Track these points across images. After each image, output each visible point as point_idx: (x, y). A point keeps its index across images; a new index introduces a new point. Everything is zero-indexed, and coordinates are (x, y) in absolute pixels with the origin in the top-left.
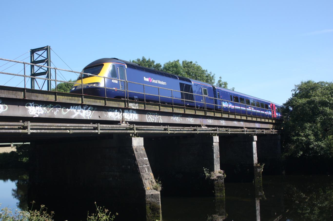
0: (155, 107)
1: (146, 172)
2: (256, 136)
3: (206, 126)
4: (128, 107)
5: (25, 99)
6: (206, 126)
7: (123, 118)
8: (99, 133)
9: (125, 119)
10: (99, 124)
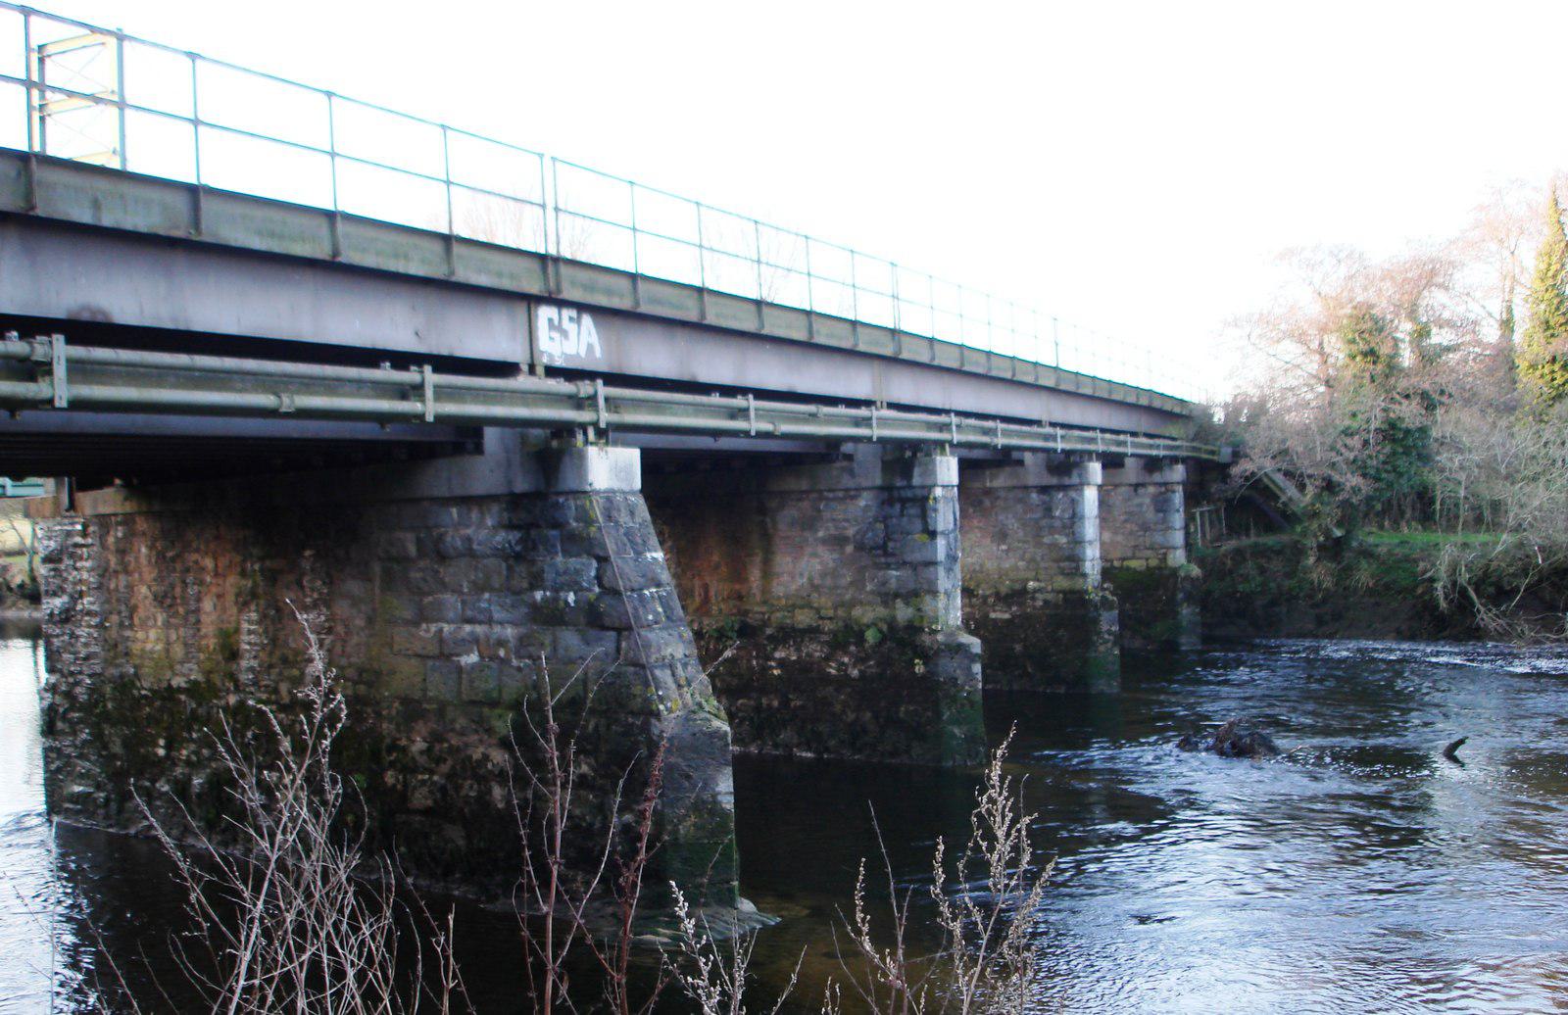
0: (500, 275)
1: (216, 760)
2: (1097, 460)
3: (892, 406)
4: (763, 327)
5: (32, 213)
6: (892, 406)
7: (535, 351)
8: (430, 418)
9: (543, 352)
10: (55, 337)
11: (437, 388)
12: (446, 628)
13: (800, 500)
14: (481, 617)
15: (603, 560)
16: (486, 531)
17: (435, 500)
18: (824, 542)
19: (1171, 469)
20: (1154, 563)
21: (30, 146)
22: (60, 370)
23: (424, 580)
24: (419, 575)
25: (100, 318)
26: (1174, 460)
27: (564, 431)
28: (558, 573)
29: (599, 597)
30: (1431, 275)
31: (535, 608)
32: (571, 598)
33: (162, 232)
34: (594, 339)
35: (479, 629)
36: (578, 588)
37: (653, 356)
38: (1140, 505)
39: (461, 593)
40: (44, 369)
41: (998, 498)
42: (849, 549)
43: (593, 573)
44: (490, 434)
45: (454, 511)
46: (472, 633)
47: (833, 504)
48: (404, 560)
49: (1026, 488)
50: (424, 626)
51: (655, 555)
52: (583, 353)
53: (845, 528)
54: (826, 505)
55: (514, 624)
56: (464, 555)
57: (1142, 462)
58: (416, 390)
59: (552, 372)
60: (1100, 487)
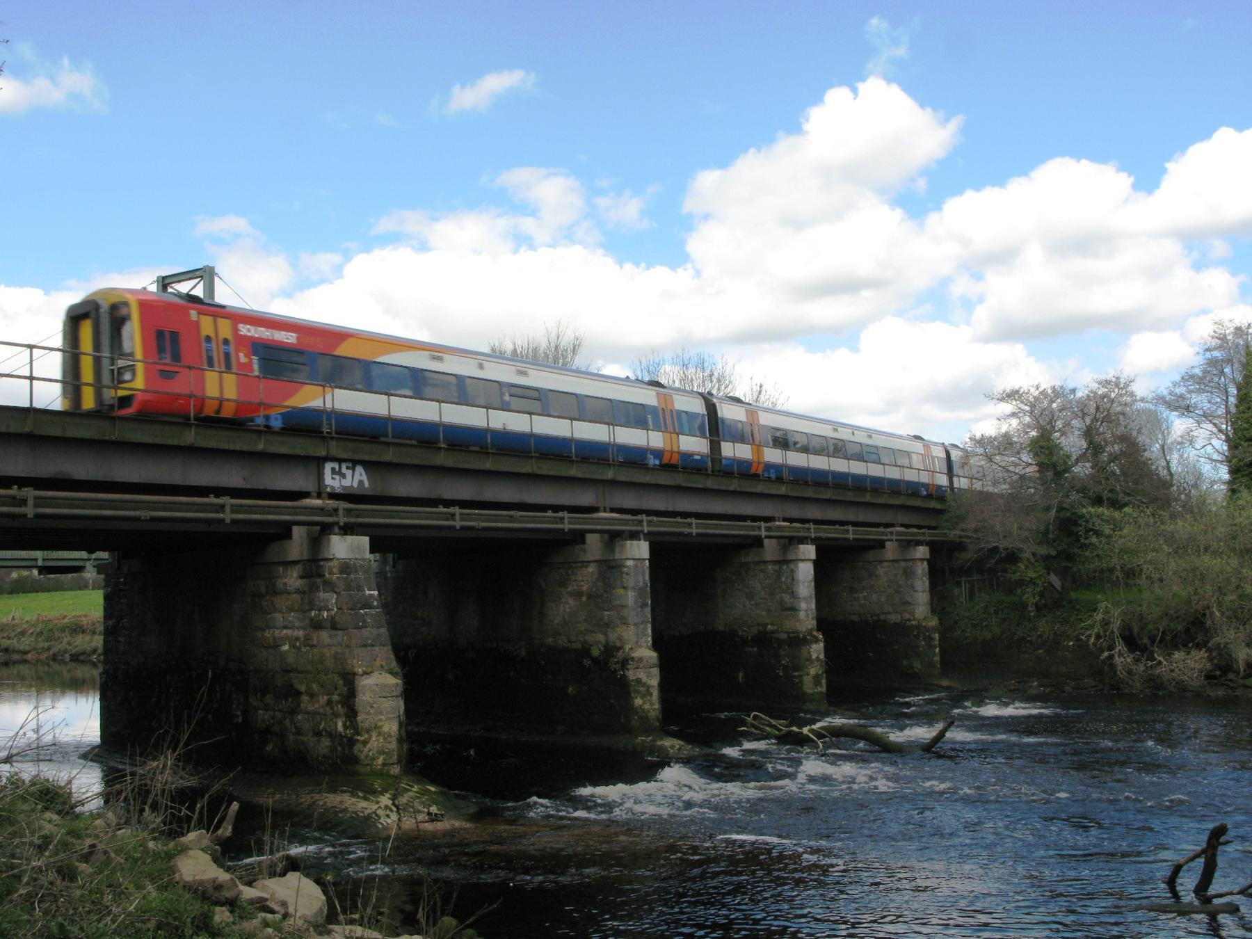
8: (228, 521)
12: (277, 632)
13: (559, 568)
19: (915, 550)
20: (761, 628)
22: (30, 502)
25: (66, 477)
29: (337, 613)
31: (312, 619)
32: (325, 614)
33: (96, 438)
34: (364, 478)
40: (23, 502)
42: (584, 599)
43: (334, 601)
45: (281, 569)
46: (286, 634)
52: (355, 485)
53: (582, 586)
55: (304, 629)
57: (606, 536)
59: (333, 496)
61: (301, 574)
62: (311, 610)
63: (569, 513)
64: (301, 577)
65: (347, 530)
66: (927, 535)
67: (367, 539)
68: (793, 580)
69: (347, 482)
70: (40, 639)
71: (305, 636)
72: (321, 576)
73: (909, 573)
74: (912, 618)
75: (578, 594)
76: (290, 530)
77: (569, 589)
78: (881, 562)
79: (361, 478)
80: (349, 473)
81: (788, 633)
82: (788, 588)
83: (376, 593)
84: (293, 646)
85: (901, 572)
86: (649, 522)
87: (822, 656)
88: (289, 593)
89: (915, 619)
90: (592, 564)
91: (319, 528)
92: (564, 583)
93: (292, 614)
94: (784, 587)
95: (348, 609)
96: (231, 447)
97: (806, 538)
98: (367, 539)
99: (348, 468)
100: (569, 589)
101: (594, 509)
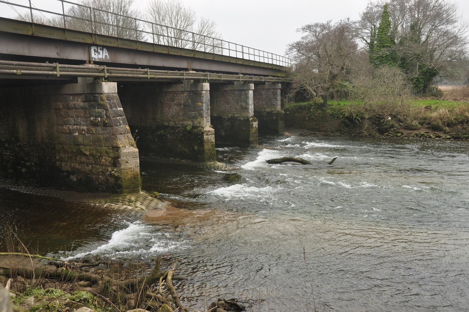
7: (90, 57)
8: (58, 76)
11: (107, 70)
12: (71, 127)
14: (78, 124)
15: (107, 110)
16: (79, 102)
17: (66, 94)
18: (176, 104)
20: (233, 116)
21: (65, 27)
23: (64, 114)
24: (63, 113)
26: (278, 83)
27: (97, 78)
28: (96, 113)
30: (331, 21)
31: (91, 121)
34: (107, 54)
35: (78, 127)
36: (101, 117)
37: (124, 59)
38: (269, 94)
39: (74, 118)
41: (228, 93)
42: (182, 106)
44: (79, 79)
47: (178, 95)
48: (59, 109)
49: (235, 90)
50: (65, 126)
51: (120, 109)
52: (104, 57)
54: (176, 95)
56: (74, 108)
58: (55, 69)
59: (95, 63)
60: (254, 90)
61: (84, 100)
62: (90, 117)
63: (107, 66)
64: (84, 102)
65: (109, 79)
66: (282, 80)
67: (116, 83)
68: (246, 97)
69: (100, 56)
70: (44, 146)
71: (87, 129)
72: (96, 101)
73: (275, 94)
74: (275, 110)
75: (180, 105)
76: (77, 78)
77: (175, 103)
78: (263, 89)
79: (106, 54)
80: (101, 52)
81: (244, 117)
82: (244, 100)
83: (122, 109)
84: (80, 133)
85: (271, 93)
86: (107, 70)
87: (257, 126)
88: (76, 108)
89: (276, 111)
90: (186, 92)
91: (93, 78)
92: (172, 100)
93: (80, 118)
94: (242, 100)
95: (112, 117)
96: (78, 40)
97: (251, 81)
98: (116, 83)
99: (100, 49)
100: (175, 103)
101: (186, 70)
